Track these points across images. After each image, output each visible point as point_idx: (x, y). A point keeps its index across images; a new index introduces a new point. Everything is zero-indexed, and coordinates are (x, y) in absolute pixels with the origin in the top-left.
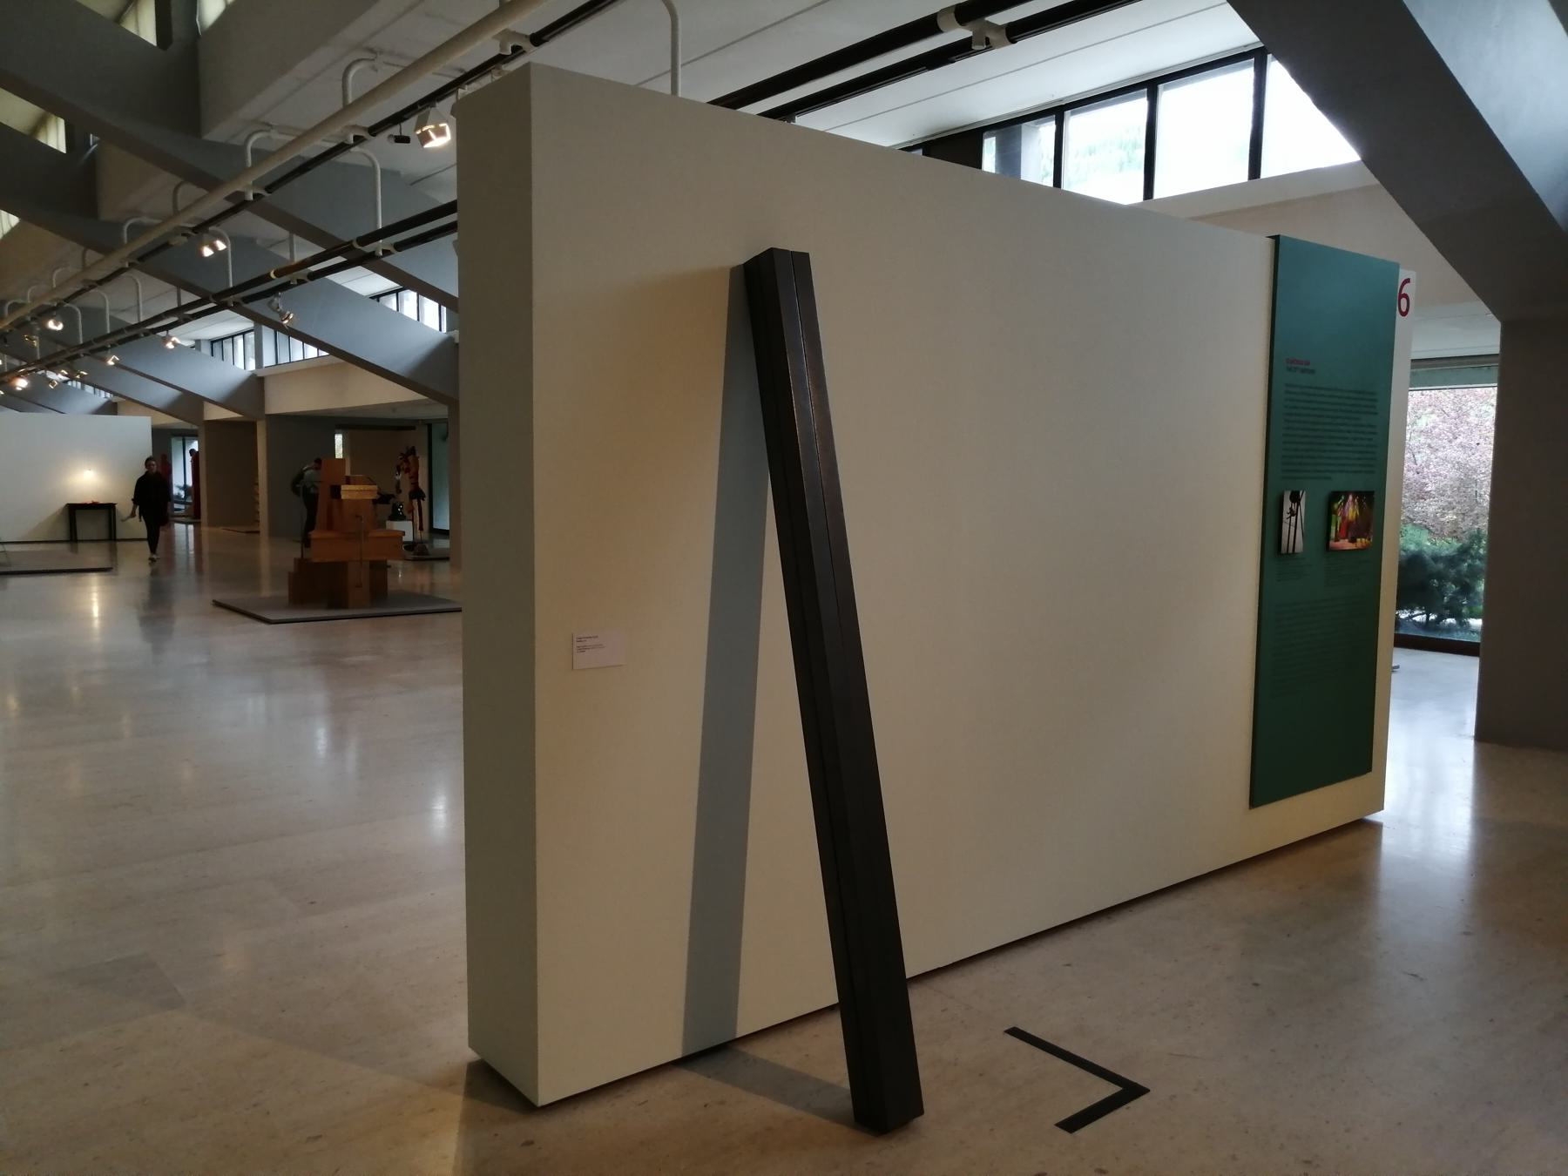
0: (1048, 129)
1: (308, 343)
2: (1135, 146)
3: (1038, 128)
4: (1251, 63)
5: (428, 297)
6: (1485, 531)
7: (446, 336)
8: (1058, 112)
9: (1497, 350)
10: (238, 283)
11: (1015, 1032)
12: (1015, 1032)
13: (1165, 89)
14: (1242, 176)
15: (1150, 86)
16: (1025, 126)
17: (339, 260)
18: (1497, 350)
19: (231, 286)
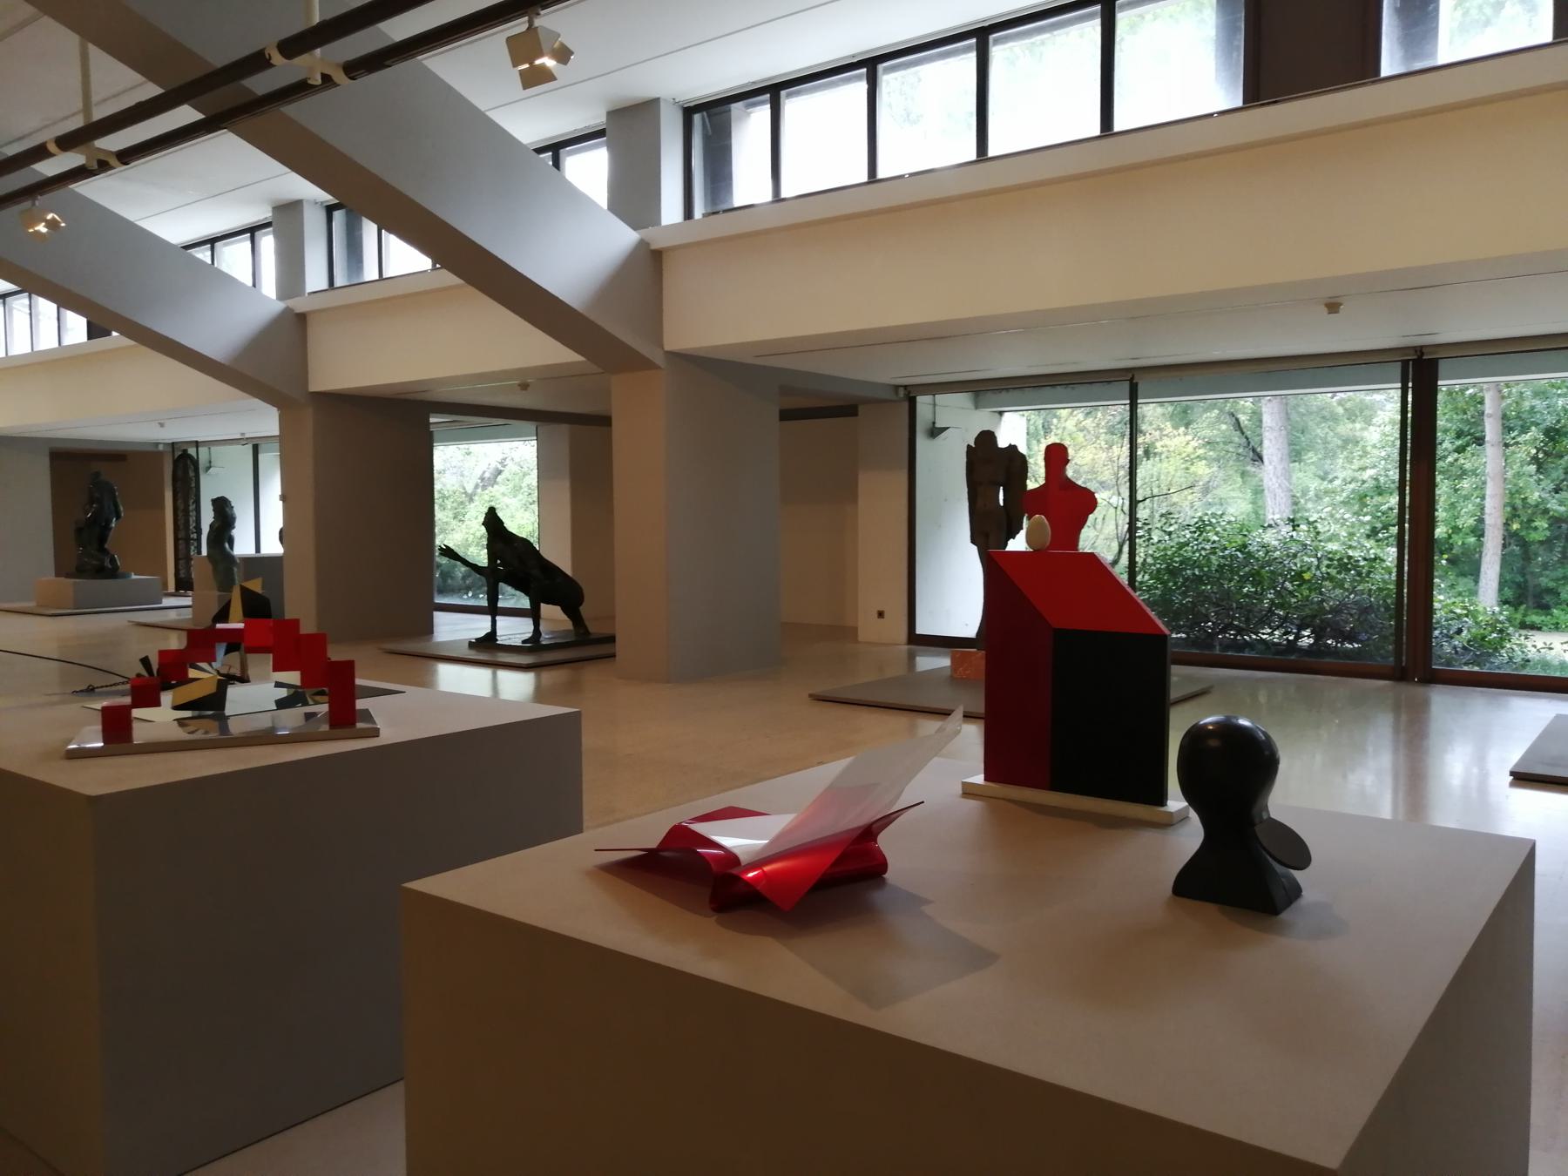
0: (760, 116)
1: (390, 231)
2: (972, 113)
3: (749, 114)
4: (861, 75)
5: (977, 56)
6: (1397, 480)
7: (281, 306)
8: (774, 92)
9: (277, 433)
10: (330, 15)
11: (596, 850)
12: (596, 850)
13: (789, 96)
14: (56, 345)
15: (870, 66)
16: (736, 107)
17: (185, 115)
18: (277, 433)
19: (317, 19)
